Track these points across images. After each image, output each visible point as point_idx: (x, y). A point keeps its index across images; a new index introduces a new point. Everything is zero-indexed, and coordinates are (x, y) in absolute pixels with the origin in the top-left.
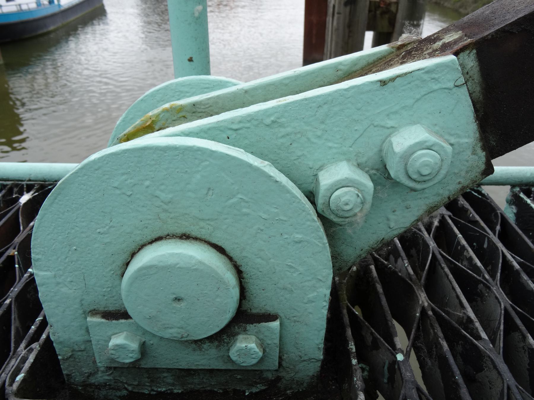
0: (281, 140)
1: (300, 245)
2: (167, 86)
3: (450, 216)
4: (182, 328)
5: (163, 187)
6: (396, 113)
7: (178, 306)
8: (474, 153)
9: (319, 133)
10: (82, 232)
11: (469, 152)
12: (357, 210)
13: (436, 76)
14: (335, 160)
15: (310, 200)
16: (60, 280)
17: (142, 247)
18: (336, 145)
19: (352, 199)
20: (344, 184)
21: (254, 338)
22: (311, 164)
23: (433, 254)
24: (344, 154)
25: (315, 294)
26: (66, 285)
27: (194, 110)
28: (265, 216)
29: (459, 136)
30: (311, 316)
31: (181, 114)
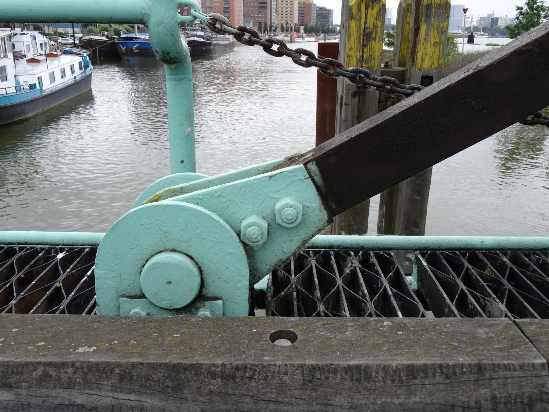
0: (223, 205)
1: (231, 255)
2: (167, 178)
3: (360, 268)
4: (170, 300)
5: (164, 224)
6: (278, 191)
7: (169, 287)
8: (321, 211)
9: (242, 201)
10: (123, 248)
11: (318, 211)
12: (259, 238)
13: (295, 174)
14: (251, 215)
15: (245, 243)
16: (108, 276)
17: (152, 256)
18: (251, 207)
19: (256, 232)
20: (252, 224)
21: (208, 310)
22: (239, 217)
23: (338, 288)
24: (255, 212)
25: (241, 284)
26: (110, 279)
27: (182, 191)
28: (213, 240)
29: (311, 203)
30: (240, 298)
31: (174, 193)
